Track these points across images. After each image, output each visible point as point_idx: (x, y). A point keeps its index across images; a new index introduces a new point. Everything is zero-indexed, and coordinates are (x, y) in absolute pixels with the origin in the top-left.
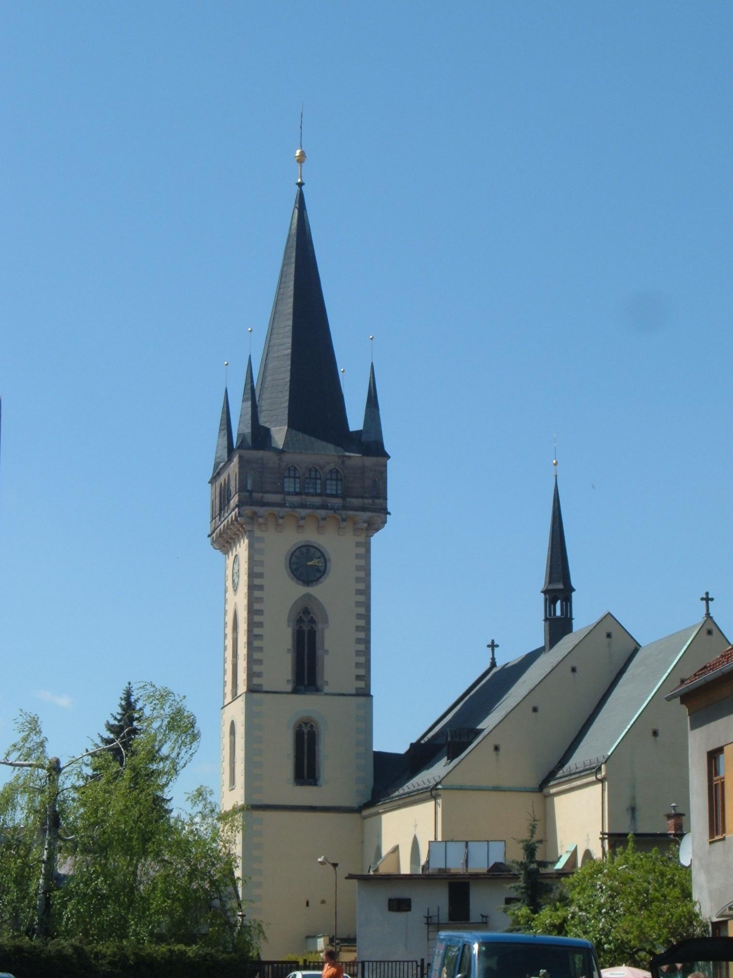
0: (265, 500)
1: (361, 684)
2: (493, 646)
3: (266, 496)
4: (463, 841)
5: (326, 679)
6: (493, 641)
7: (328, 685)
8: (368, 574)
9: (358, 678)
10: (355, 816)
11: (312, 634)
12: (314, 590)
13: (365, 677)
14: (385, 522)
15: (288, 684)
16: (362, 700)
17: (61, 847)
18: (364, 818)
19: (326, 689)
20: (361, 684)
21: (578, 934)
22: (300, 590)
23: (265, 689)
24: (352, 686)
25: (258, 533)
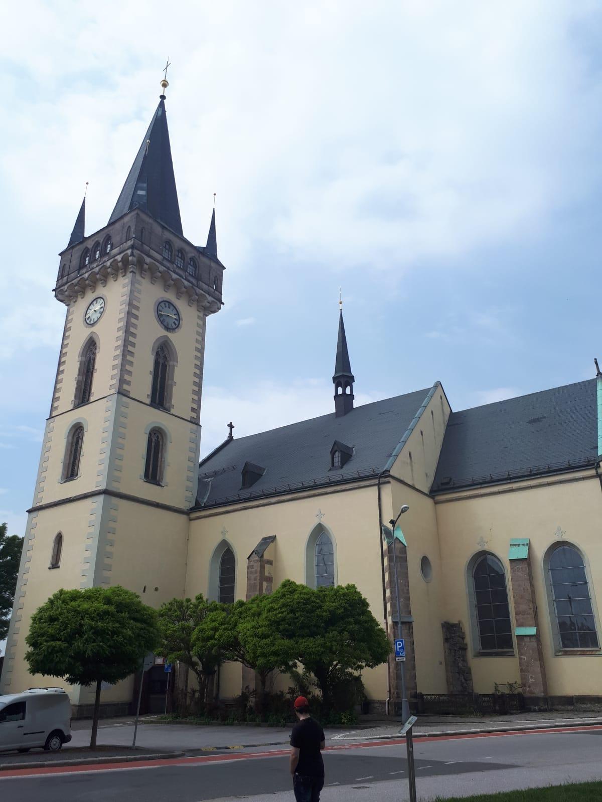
0: (151, 254)
1: (194, 415)
2: (231, 426)
3: (151, 251)
4: (397, 520)
5: (173, 403)
6: (231, 423)
7: (173, 408)
8: (203, 339)
9: (193, 410)
10: (184, 518)
11: (164, 367)
12: (170, 335)
13: (197, 410)
14: (219, 309)
15: (148, 397)
16: (195, 426)
17: (195, 691)
18: (191, 520)
19: (173, 411)
20: (194, 415)
21: (306, 605)
22: (164, 333)
23: (131, 396)
24: (189, 415)
25: (138, 277)
